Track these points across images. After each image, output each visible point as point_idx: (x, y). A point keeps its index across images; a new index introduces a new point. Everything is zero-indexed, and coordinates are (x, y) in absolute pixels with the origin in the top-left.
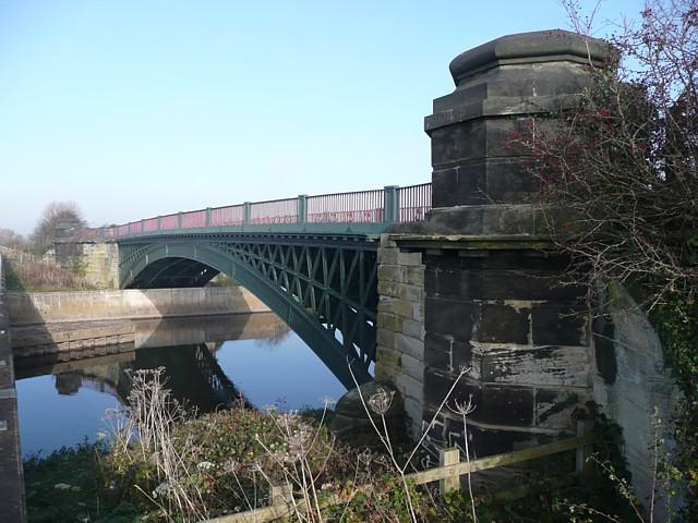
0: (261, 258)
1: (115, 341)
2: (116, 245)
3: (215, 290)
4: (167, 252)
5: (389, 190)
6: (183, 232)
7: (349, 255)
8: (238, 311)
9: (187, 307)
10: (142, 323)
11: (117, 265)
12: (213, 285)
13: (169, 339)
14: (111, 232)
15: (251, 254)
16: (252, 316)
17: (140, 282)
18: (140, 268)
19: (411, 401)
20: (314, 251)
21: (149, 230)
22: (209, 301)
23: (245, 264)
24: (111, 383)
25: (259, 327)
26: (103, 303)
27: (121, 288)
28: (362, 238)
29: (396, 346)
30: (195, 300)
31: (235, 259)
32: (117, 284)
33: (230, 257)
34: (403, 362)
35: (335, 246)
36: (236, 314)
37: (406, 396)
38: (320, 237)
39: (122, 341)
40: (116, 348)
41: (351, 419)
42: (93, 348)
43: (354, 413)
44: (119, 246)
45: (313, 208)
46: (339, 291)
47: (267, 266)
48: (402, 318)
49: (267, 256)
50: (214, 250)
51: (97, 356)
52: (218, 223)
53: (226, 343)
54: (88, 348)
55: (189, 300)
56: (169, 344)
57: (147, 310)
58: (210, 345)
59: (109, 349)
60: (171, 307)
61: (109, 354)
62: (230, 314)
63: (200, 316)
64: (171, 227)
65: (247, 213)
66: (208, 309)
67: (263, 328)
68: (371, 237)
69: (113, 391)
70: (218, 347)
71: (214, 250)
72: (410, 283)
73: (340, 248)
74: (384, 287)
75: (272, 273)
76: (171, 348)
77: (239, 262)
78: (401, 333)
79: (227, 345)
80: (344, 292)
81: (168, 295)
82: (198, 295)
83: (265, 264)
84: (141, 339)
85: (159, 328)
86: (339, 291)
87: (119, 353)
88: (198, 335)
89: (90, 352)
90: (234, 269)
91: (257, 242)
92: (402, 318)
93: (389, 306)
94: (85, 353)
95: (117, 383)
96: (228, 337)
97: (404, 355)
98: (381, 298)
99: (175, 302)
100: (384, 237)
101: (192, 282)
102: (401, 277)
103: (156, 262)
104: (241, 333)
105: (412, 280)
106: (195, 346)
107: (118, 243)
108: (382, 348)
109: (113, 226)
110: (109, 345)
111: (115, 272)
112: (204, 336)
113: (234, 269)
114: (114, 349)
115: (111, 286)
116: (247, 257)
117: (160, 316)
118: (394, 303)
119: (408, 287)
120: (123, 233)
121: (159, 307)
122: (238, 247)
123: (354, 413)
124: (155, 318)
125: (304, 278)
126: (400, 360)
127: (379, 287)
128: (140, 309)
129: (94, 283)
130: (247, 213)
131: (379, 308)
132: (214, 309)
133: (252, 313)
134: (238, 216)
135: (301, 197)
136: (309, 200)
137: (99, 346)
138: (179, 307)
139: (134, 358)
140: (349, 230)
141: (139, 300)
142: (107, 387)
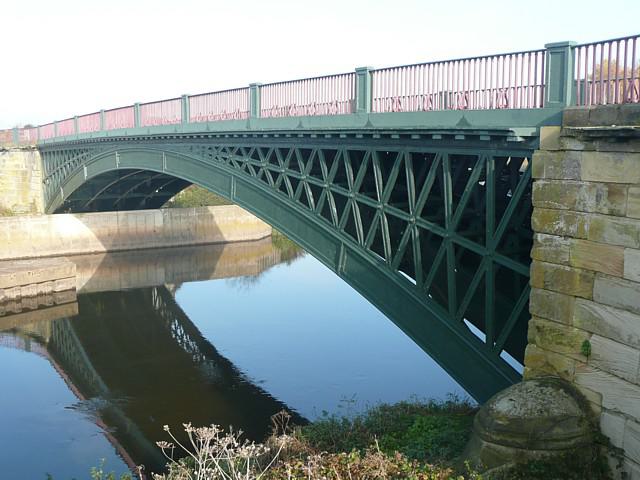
0: (283, 169)
1: (48, 289)
2: (37, 153)
3: (176, 212)
4: (118, 162)
5: (361, 73)
6: (144, 132)
7: (461, 166)
8: (208, 240)
9: (140, 236)
10: (82, 259)
11: (39, 180)
12: (172, 206)
13: (117, 281)
14: (27, 134)
15: (264, 164)
16: (226, 248)
17: (76, 204)
18: (72, 187)
19: (614, 418)
20: (387, 160)
21: (88, 130)
22: (169, 226)
23: (254, 179)
24: (39, 340)
25: (236, 261)
26: (26, 233)
27: (46, 212)
28: (500, 136)
29: (575, 320)
30: (150, 227)
31: (238, 171)
32: (41, 206)
33: (226, 168)
34: (595, 349)
35: (395, 149)
36: (205, 244)
37: (604, 409)
38: (405, 135)
39: (58, 288)
40: (51, 298)
41: (511, 451)
42: (19, 300)
43: (519, 441)
44: (42, 154)
45: (269, 102)
46: (441, 223)
47: (295, 182)
48: (589, 276)
49: (294, 166)
50: (197, 157)
51: (26, 310)
52: (209, 114)
53: (185, 284)
54: (12, 300)
55: (141, 227)
56: (117, 288)
57: (85, 242)
58: (170, 287)
59: (41, 301)
60: (118, 237)
61: (41, 307)
62: (197, 245)
63: (157, 248)
64: (120, 125)
65: (255, 101)
66: (168, 239)
67: (242, 262)
68: (520, 133)
69: (44, 350)
70: (177, 287)
71: (197, 157)
72: (612, 214)
73: (343, 149)
74: (545, 220)
75: (326, 203)
76: (120, 293)
77: (244, 177)
78: (591, 299)
79: (186, 286)
80: (451, 224)
81: (114, 221)
82: (152, 221)
83: (313, 187)
84: (81, 280)
85: (103, 266)
86: (441, 223)
87: (55, 305)
88: (155, 275)
89: (16, 307)
90: (234, 187)
91: (256, 146)
92: (589, 276)
93: (558, 253)
94: (9, 308)
95: (48, 340)
96: (196, 276)
97: (594, 337)
98: (540, 237)
99: (122, 231)
100: (546, 133)
101: (144, 202)
102: (591, 203)
103: (97, 178)
104: (212, 269)
105: (621, 208)
106: (150, 289)
107: (40, 149)
108: (540, 322)
109: (28, 127)
110: (41, 295)
111: (37, 191)
112: (163, 275)
113: (234, 187)
114: (48, 300)
115: (33, 208)
116: (240, 163)
117: (104, 249)
118: (571, 246)
119: (609, 221)
120: (47, 136)
121: (101, 238)
122: (239, 153)
123: (519, 441)
124: (96, 253)
125: (369, 202)
126: (586, 345)
127: (535, 220)
128: (75, 241)
129: (9, 206)
130: (255, 101)
131: (535, 253)
132: (176, 238)
133: (226, 243)
134: (240, 104)
135: (253, 86)
136: (192, 99)
137: (27, 297)
138: (129, 236)
139: (77, 312)
140: (463, 121)
141: (81, 231)
142: (33, 345)
